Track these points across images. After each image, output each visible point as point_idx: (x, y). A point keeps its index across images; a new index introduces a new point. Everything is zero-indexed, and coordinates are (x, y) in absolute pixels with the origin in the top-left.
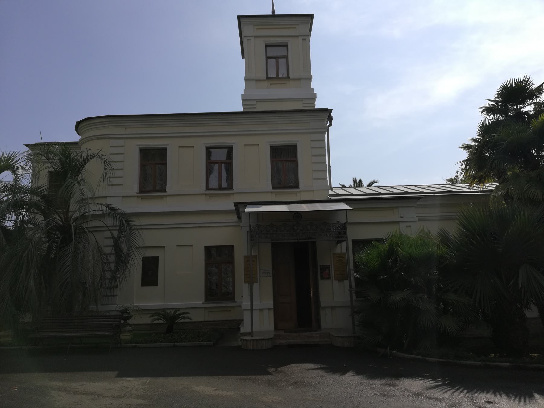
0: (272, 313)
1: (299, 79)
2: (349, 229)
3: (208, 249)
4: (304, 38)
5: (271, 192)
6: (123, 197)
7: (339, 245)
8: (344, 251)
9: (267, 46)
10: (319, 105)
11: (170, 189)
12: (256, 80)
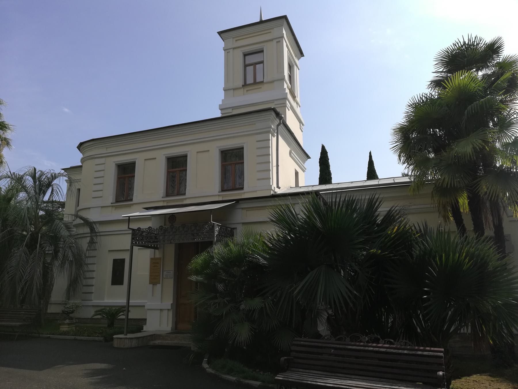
0: (171, 313)
1: (272, 82)
4: (277, 40)
6: (102, 207)
9: (245, 55)
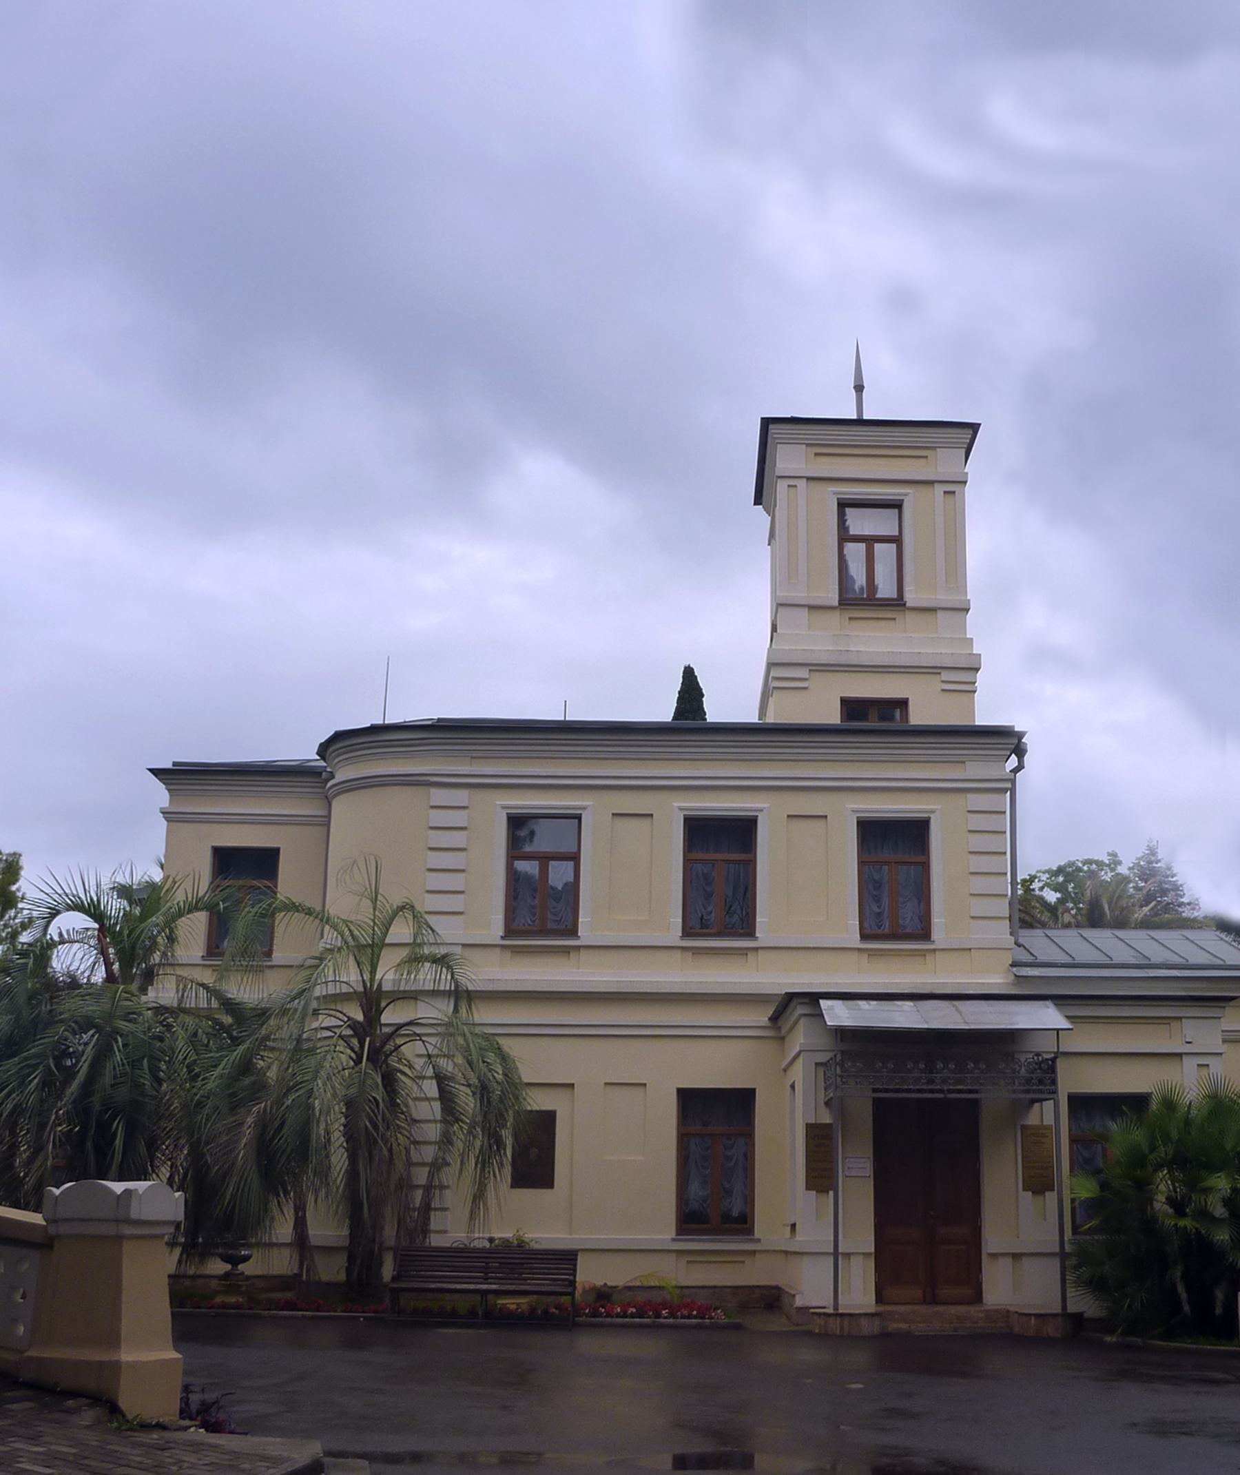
0: (871, 1264)
2: (1061, 1065)
3: (688, 1098)
5: (859, 950)
7: (1037, 1105)
8: (1049, 1120)
9: (843, 505)
10: (987, 711)
11: (588, 930)
12: (812, 608)
